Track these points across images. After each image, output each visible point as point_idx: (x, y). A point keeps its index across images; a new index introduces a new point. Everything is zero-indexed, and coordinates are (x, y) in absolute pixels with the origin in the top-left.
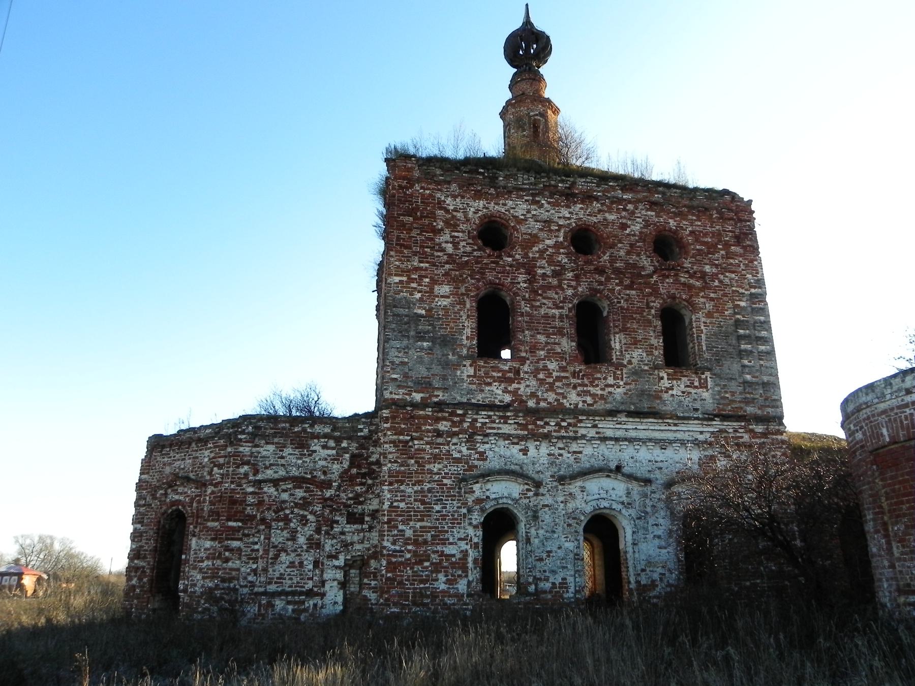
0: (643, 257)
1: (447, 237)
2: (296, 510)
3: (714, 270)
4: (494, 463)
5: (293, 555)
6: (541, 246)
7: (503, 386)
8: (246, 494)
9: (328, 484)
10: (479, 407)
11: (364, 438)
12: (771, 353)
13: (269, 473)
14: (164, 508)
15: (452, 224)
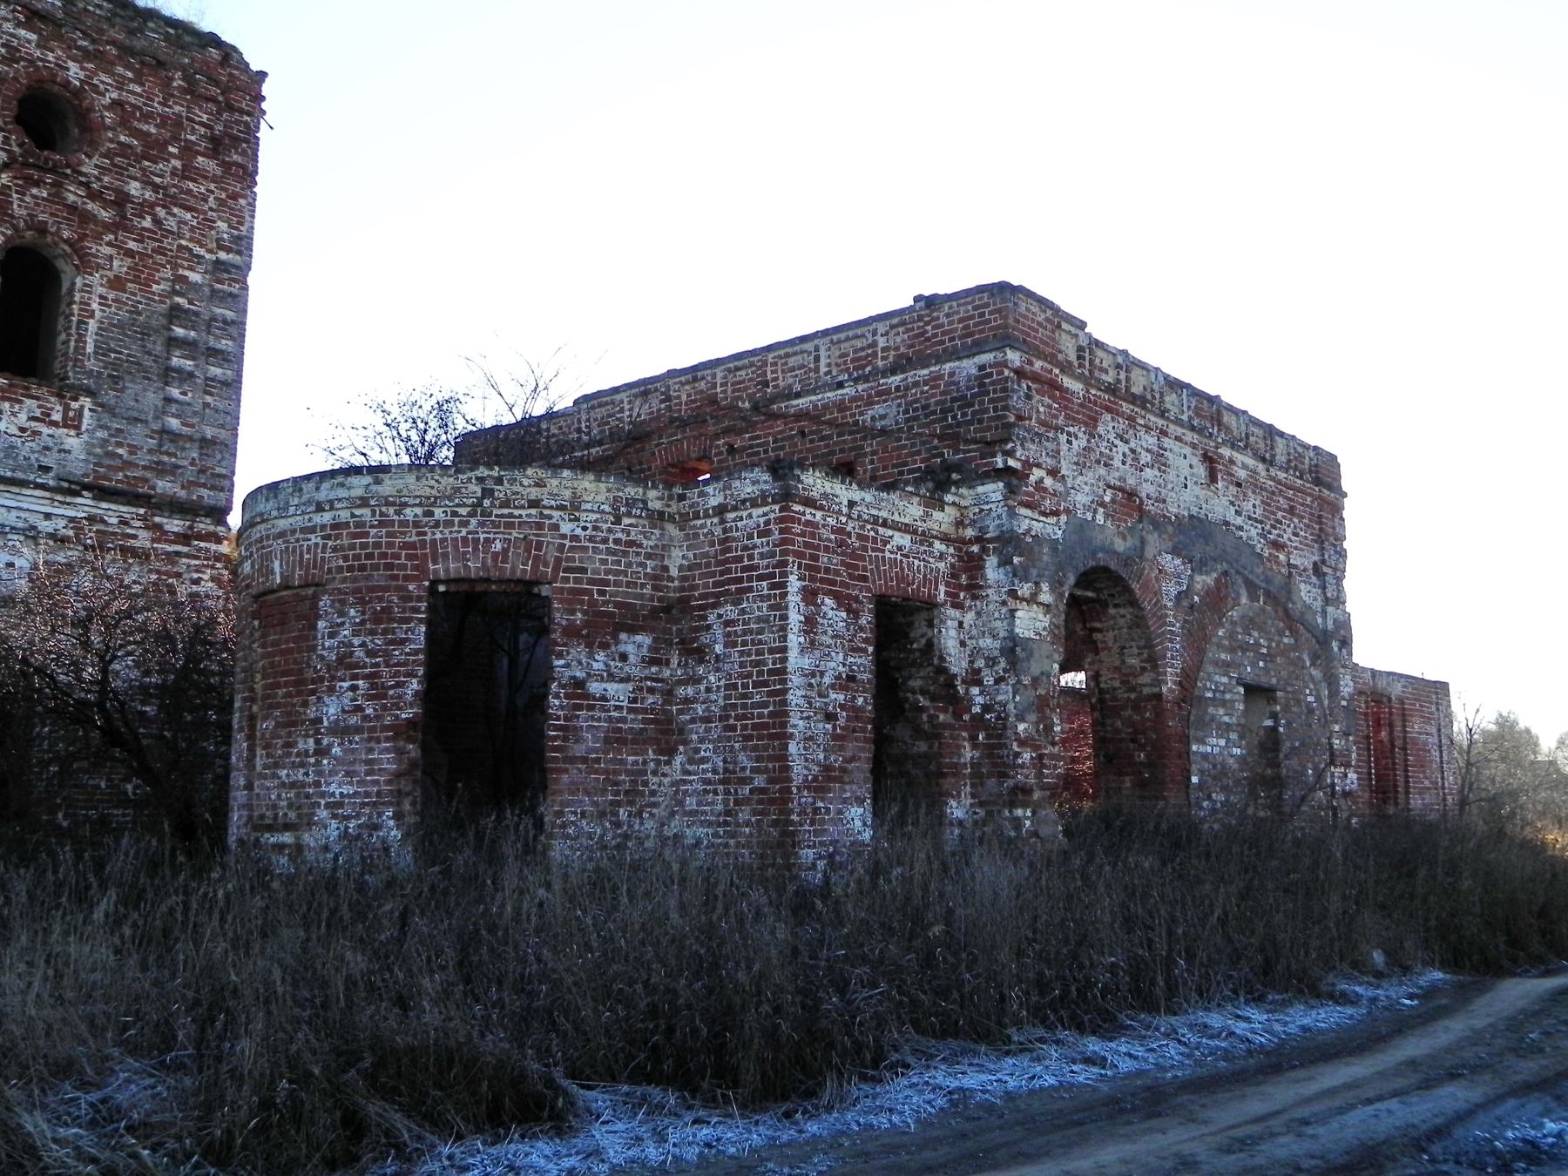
12: (233, 386)
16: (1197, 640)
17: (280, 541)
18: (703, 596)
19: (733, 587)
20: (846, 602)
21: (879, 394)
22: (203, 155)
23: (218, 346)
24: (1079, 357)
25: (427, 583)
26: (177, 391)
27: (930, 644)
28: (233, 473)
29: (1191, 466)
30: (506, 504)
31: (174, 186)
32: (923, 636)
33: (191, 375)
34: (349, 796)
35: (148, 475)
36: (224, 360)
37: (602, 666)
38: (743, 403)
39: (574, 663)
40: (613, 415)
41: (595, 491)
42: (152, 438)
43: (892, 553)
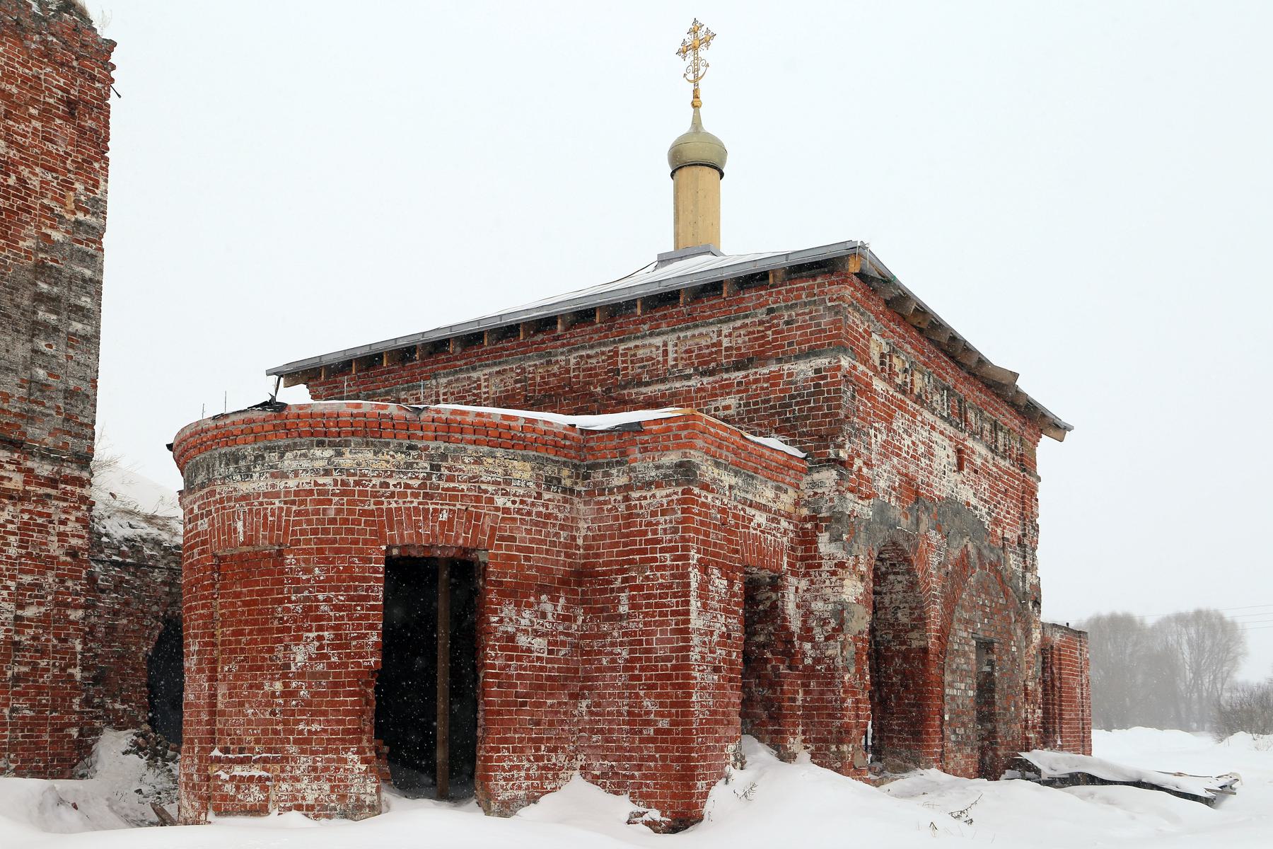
12: (91, 341)
16: (951, 603)
17: (243, 503)
18: (605, 564)
19: (637, 557)
20: (727, 573)
21: (722, 387)
22: (60, 117)
23: (79, 303)
24: (881, 364)
25: (384, 548)
26: (43, 343)
27: (774, 606)
28: (94, 422)
29: (948, 456)
30: (450, 479)
31: (35, 146)
32: (768, 598)
34: (316, 732)
35: (20, 422)
36: (84, 316)
37: (528, 623)
38: (595, 388)
39: (507, 620)
40: (469, 391)
41: (523, 471)
42: (21, 387)
43: (755, 529)
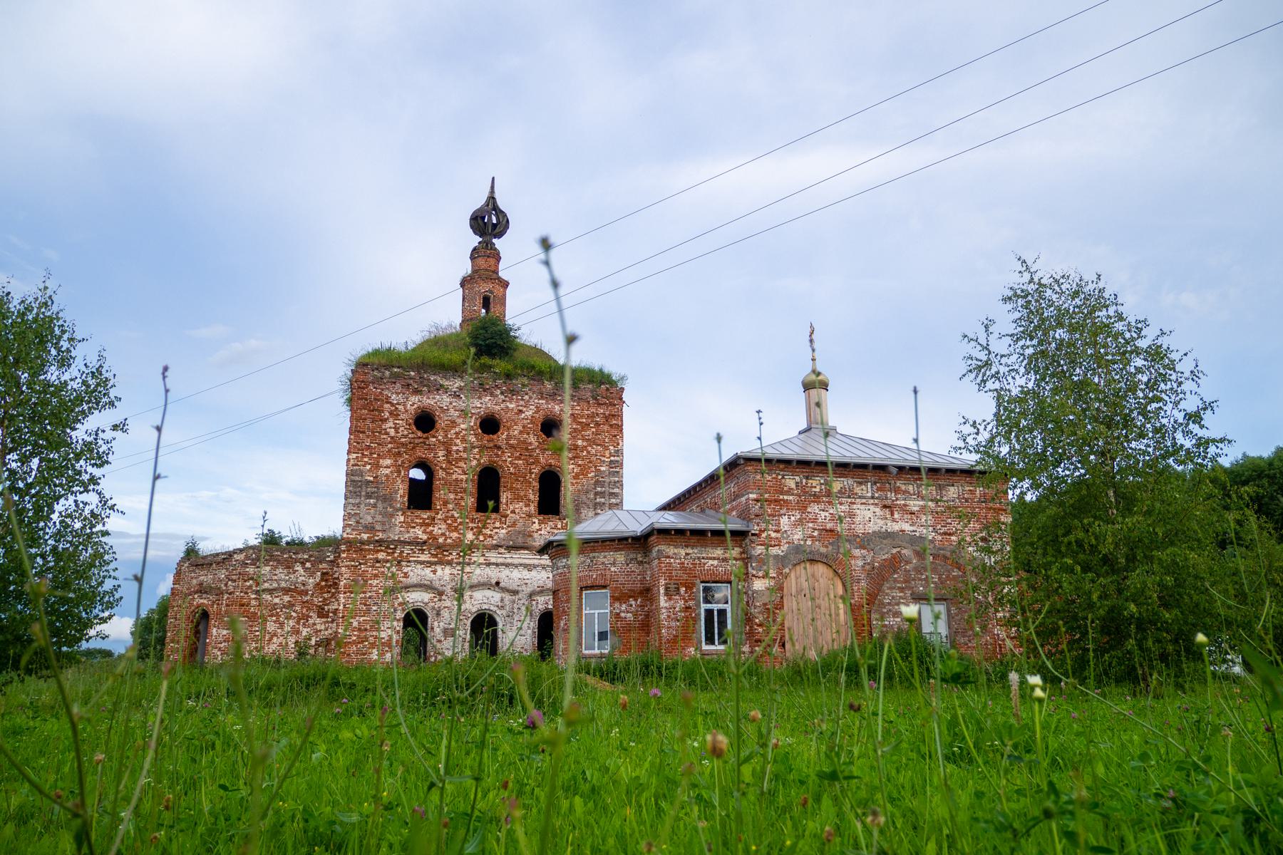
0: (531, 436)
1: (391, 424)
2: (284, 610)
3: (585, 444)
4: (413, 579)
5: (281, 638)
6: (457, 429)
7: (423, 528)
8: (250, 599)
9: (306, 593)
10: (405, 543)
11: (331, 561)
13: (266, 585)
14: (193, 608)
15: (394, 414)
33: (604, 504)
41: (620, 557)
